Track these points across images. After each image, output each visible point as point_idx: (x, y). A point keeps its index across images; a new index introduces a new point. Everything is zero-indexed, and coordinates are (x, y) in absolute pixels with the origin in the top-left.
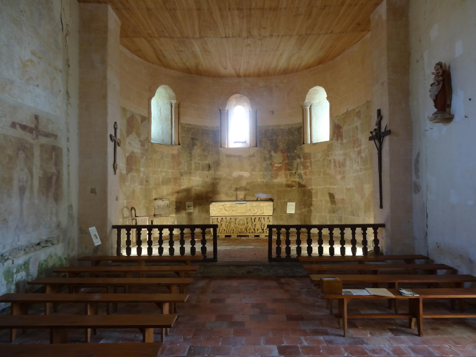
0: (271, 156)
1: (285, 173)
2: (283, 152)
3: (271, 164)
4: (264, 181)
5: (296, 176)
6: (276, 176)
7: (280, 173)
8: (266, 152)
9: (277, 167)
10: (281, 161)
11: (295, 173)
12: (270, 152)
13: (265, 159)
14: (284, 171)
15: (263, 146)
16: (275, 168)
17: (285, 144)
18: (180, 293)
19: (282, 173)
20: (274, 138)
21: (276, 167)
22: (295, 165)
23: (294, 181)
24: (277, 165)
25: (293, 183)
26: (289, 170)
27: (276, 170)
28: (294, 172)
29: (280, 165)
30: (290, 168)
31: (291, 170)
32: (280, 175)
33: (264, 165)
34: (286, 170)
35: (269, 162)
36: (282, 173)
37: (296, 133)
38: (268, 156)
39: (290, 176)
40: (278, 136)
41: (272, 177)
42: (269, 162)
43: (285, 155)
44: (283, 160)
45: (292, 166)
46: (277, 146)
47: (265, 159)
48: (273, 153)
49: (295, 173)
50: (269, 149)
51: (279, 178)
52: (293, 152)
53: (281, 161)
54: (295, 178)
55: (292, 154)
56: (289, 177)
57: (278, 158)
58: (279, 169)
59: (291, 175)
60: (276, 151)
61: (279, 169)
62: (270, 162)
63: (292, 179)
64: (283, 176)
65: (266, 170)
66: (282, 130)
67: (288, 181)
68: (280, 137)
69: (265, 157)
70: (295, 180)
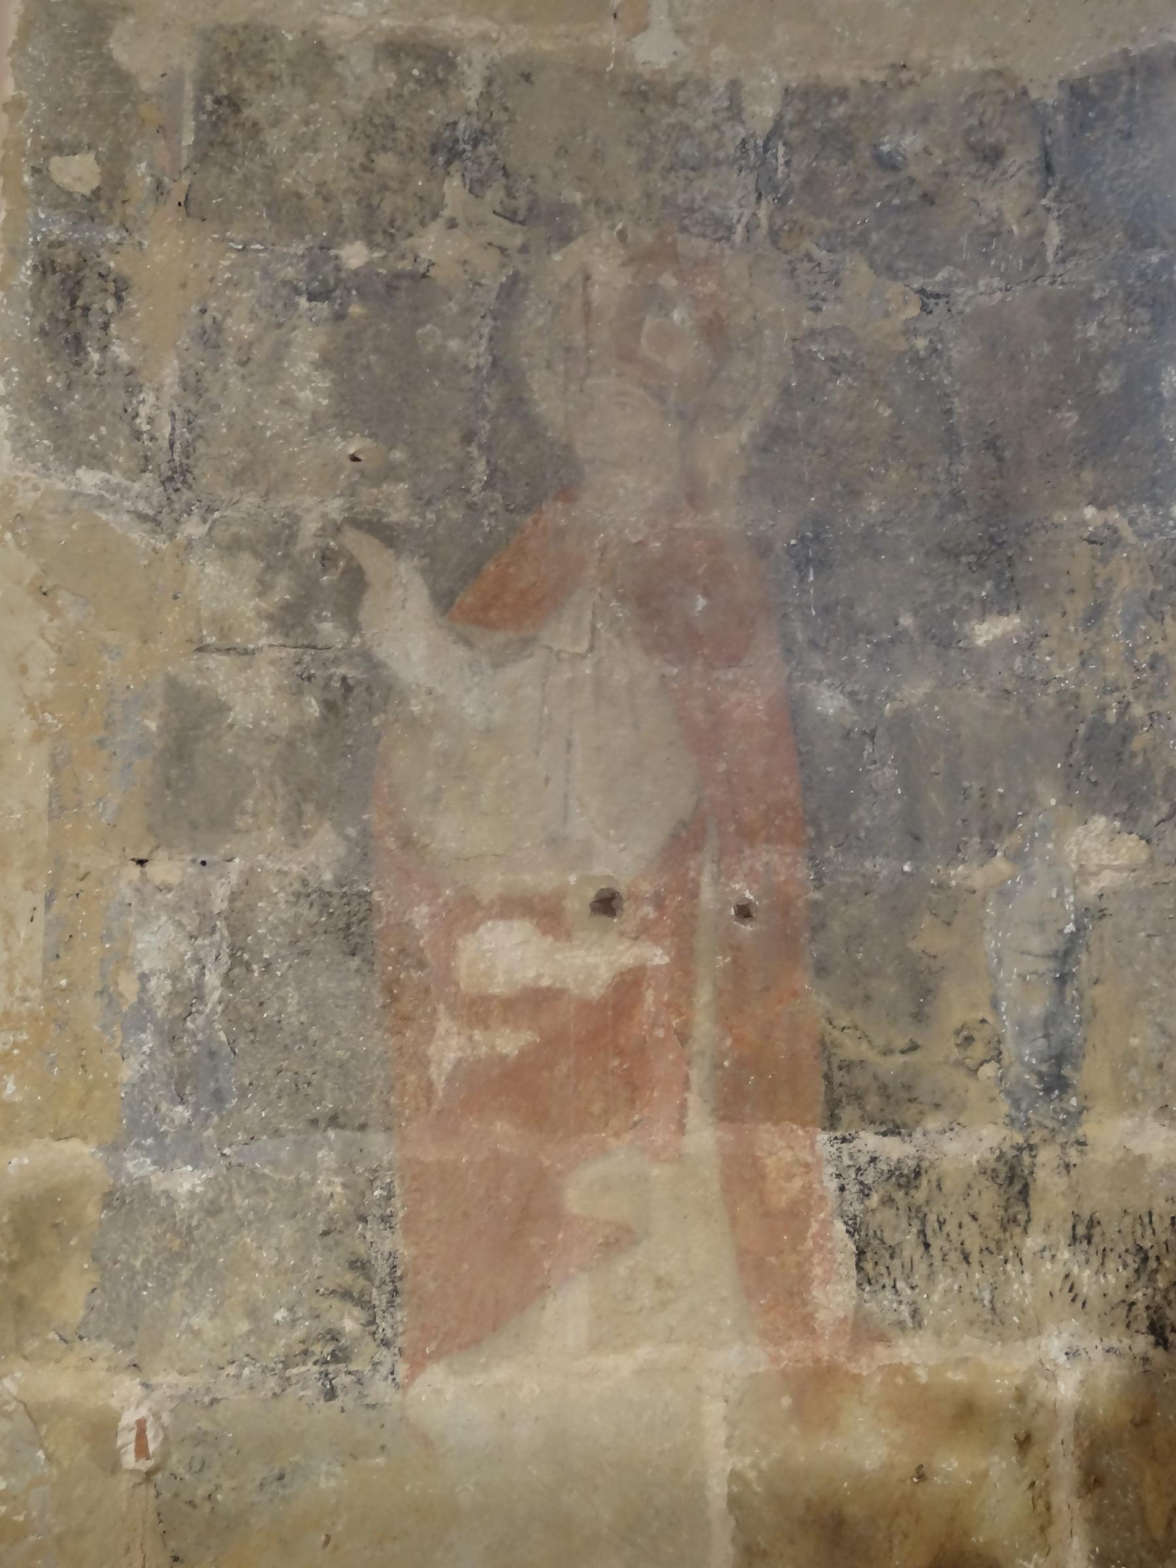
0: (351, 707)
1: (742, 1175)
2: (651, 598)
3: (347, 923)
4: (130, 1402)
5: (1045, 1260)
6: (511, 1245)
7: (596, 1179)
8: (224, 589)
9: (534, 1001)
10: (623, 862)
11: (1013, 1179)
12: (322, 588)
13: (186, 776)
14: (703, 1137)
15: (156, 409)
16: (449, 1047)
17: (727, 445)
18: (786, 91)
19: (656, 1174)
20: (432, 245)
21: (478, 1011)
22: (1002, 976)
23: (966, 1414)
24: (506, 955)
25: (953, 1464)
26: (840, 1098)
27: (514, 1088)
28: (963, 1146)
29: (591, 963)
30: (870, 1047)
31: (894, 1109)
32: (619, 1240)
33: (156, 946)
34: (744, 1095)
35: (283, 860)
36: (656, 1174)
37: (1007, 198)
38: (256, 696)
39: (868, 1253)
40: (554, 224)
41: (368, 1284)
42: (283, 860)
43: (750, 691)
44: (683, 842)
45: (922, 990)
46: (538, 473)
47: (186, 776)
48: (407, 634)
49: (1013, 1179)
50: (316, 512)
51: (569, 1308)
52: (943, 638)
53: (623, 862)
54: (995, 1320)
55: (915, 690)
56: (835, 1296)
57: (545, 794)
58: (588, 1059)
59: (894, 1226)
60: (487, 594)
61: (588, 1059)
62: (323, 853)
63: (916, 1353)
64: (695, 1248)
65: (195, 1075)
66: (643, 93)
67: (815, 1390)
68: (599, 262)
69: (191, 721)
70: (1001, 1367)
